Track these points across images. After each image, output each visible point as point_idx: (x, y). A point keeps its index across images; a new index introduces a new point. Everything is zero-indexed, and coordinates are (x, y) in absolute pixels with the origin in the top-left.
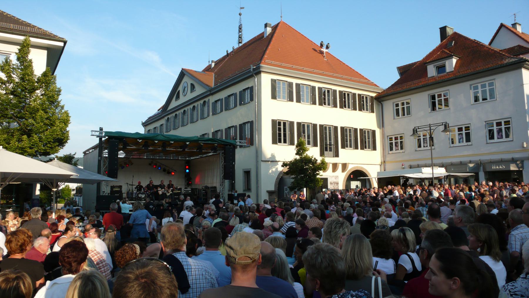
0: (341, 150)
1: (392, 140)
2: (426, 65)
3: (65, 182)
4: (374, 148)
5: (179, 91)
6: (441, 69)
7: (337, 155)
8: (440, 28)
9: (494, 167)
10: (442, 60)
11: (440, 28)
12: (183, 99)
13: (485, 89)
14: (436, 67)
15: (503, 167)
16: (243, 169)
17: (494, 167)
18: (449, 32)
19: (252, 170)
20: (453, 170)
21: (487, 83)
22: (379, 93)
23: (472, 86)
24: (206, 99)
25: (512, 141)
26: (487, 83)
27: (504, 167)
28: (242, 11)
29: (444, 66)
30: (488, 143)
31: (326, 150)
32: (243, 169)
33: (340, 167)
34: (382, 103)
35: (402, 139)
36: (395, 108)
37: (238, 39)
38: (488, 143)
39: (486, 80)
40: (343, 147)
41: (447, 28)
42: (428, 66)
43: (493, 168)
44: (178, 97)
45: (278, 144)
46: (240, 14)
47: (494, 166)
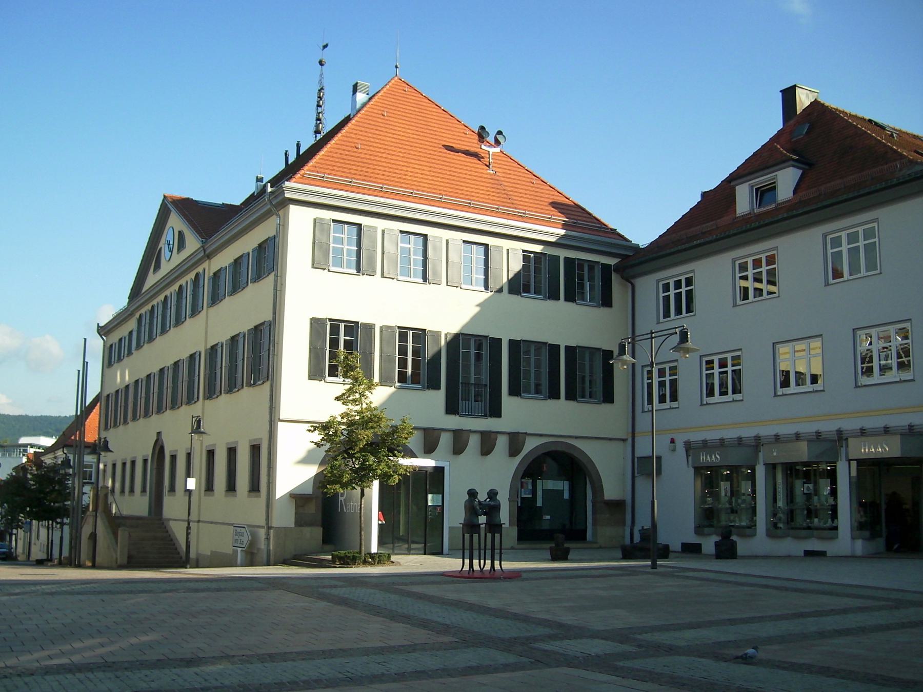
0: (508, 402)
1: (720, 373)
2: (732, 184)
3: (336, 485)
4: (608, 397)
5: (161, 248)
6: (765, 193)
7: (495, 411)
8: (781, 91)
9: (865, 449)
10: (752, 176)
11: (781, 91)
12: (166, 267)
13: (840, 249)
14: (757, 190)
15: (885, 450)
16: (250, 441)
17: (865, 449)
18: (803, 99)
19: (239, 444)
20: (775, 454)
21: (844, 234)
22: (627, 256)
23: (829, 237)
24: (200, 269)
25: (913, 380)
26: (844, 234)
27: (887, 449)
28: (326, 55)
29: (771, 189)
30: (859, 387)
31: (467, 399)
32: (227, 444)
33: (502, 443)
34: (632, 281)
35: (676, 374)
36: (662, 295)
37: (315, 122)
38: (859, 387)
39: (858, 223)
40: (515, 391)
41: (798, 90)
42: (737, 187)
43: (863, 450)
44: (158, 267)
45: (329, 379)
46: (321, 63)
47: (865, 446)
